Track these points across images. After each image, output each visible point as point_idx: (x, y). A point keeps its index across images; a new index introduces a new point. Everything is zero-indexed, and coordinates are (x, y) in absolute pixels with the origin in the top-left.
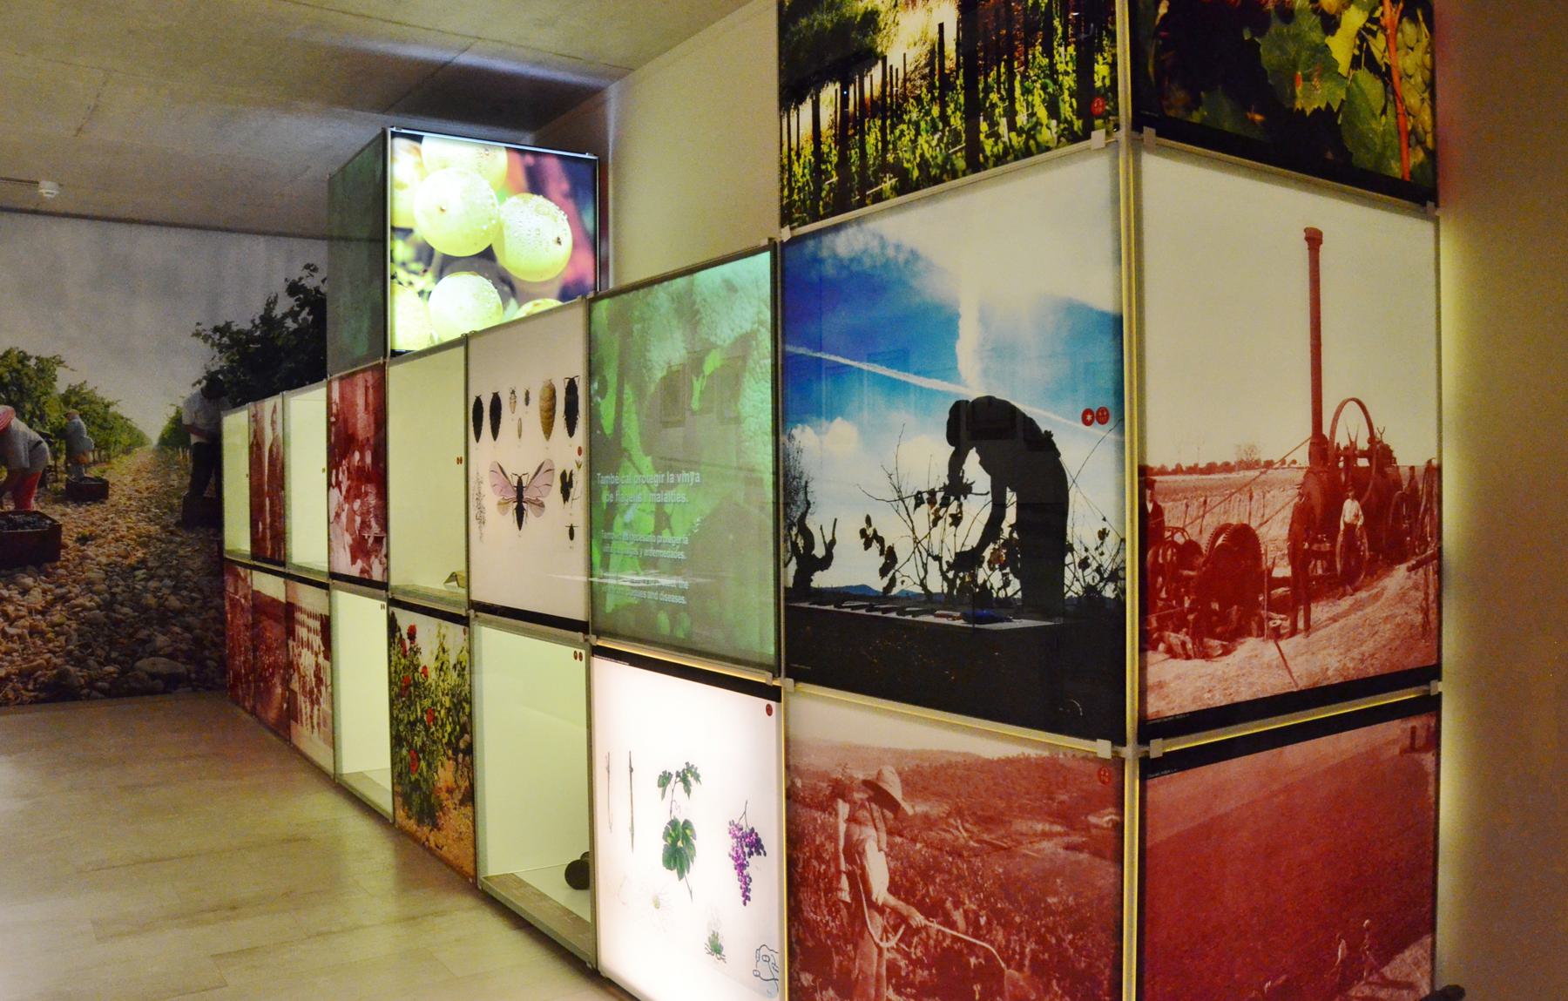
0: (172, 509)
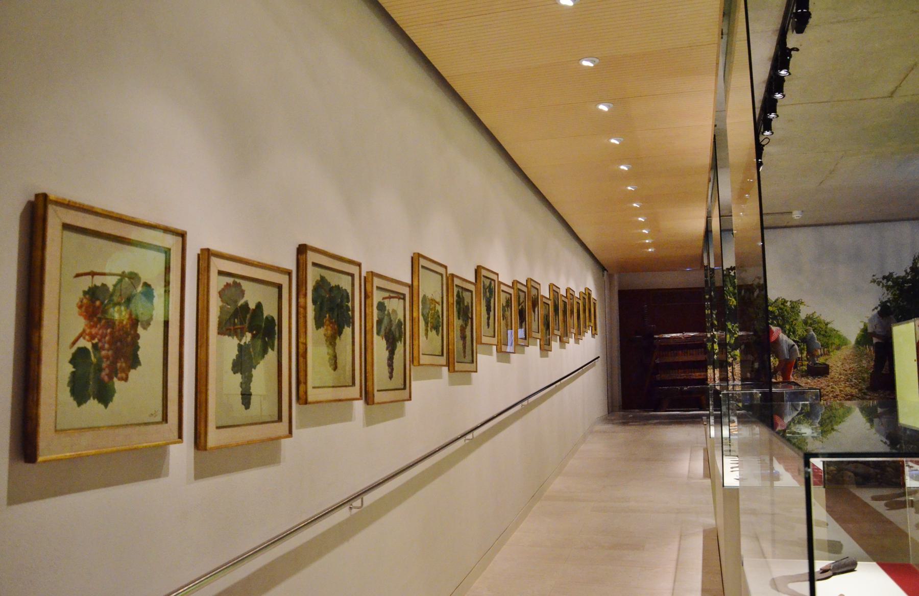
0: (863, 379)
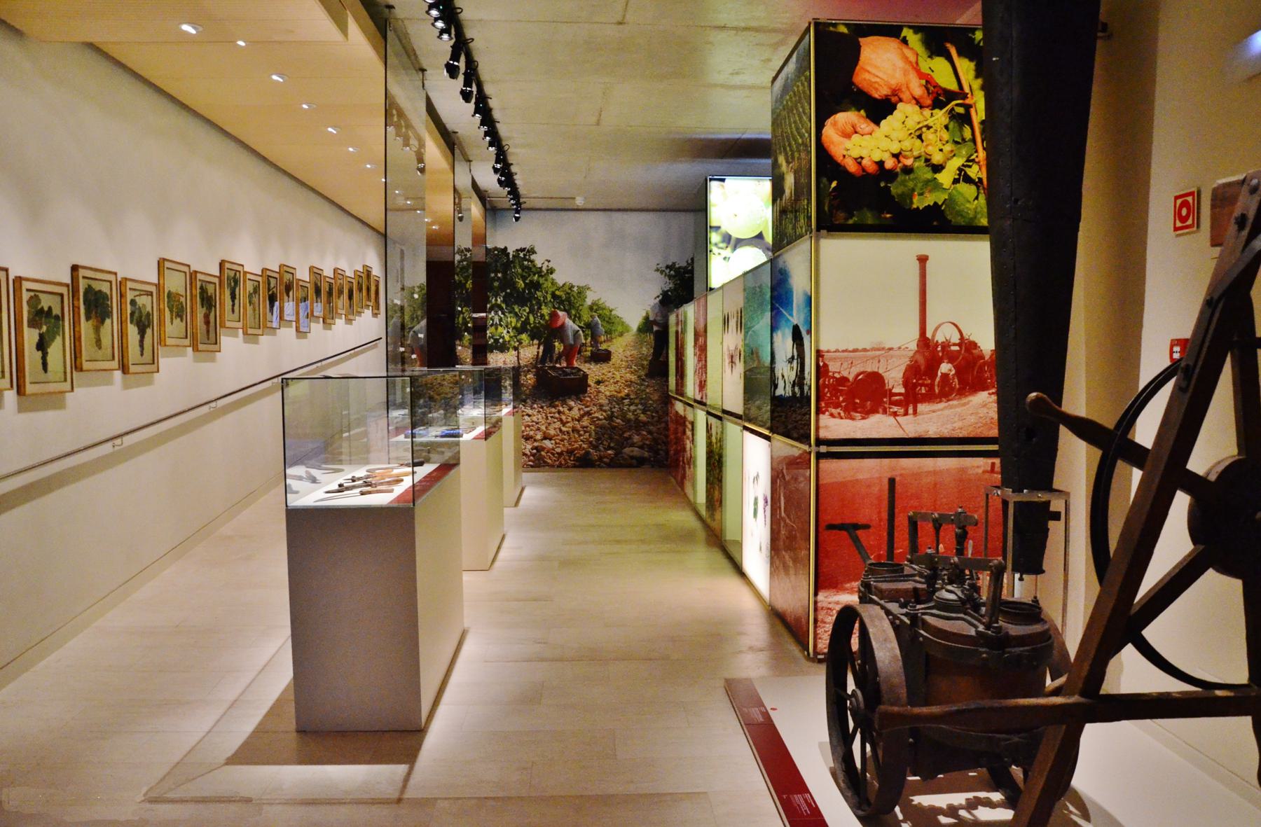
0: (642, 365)
